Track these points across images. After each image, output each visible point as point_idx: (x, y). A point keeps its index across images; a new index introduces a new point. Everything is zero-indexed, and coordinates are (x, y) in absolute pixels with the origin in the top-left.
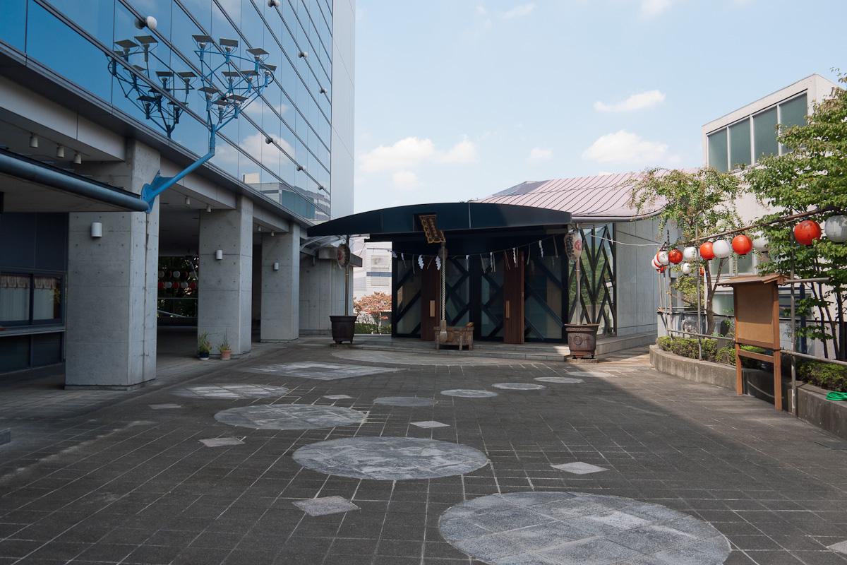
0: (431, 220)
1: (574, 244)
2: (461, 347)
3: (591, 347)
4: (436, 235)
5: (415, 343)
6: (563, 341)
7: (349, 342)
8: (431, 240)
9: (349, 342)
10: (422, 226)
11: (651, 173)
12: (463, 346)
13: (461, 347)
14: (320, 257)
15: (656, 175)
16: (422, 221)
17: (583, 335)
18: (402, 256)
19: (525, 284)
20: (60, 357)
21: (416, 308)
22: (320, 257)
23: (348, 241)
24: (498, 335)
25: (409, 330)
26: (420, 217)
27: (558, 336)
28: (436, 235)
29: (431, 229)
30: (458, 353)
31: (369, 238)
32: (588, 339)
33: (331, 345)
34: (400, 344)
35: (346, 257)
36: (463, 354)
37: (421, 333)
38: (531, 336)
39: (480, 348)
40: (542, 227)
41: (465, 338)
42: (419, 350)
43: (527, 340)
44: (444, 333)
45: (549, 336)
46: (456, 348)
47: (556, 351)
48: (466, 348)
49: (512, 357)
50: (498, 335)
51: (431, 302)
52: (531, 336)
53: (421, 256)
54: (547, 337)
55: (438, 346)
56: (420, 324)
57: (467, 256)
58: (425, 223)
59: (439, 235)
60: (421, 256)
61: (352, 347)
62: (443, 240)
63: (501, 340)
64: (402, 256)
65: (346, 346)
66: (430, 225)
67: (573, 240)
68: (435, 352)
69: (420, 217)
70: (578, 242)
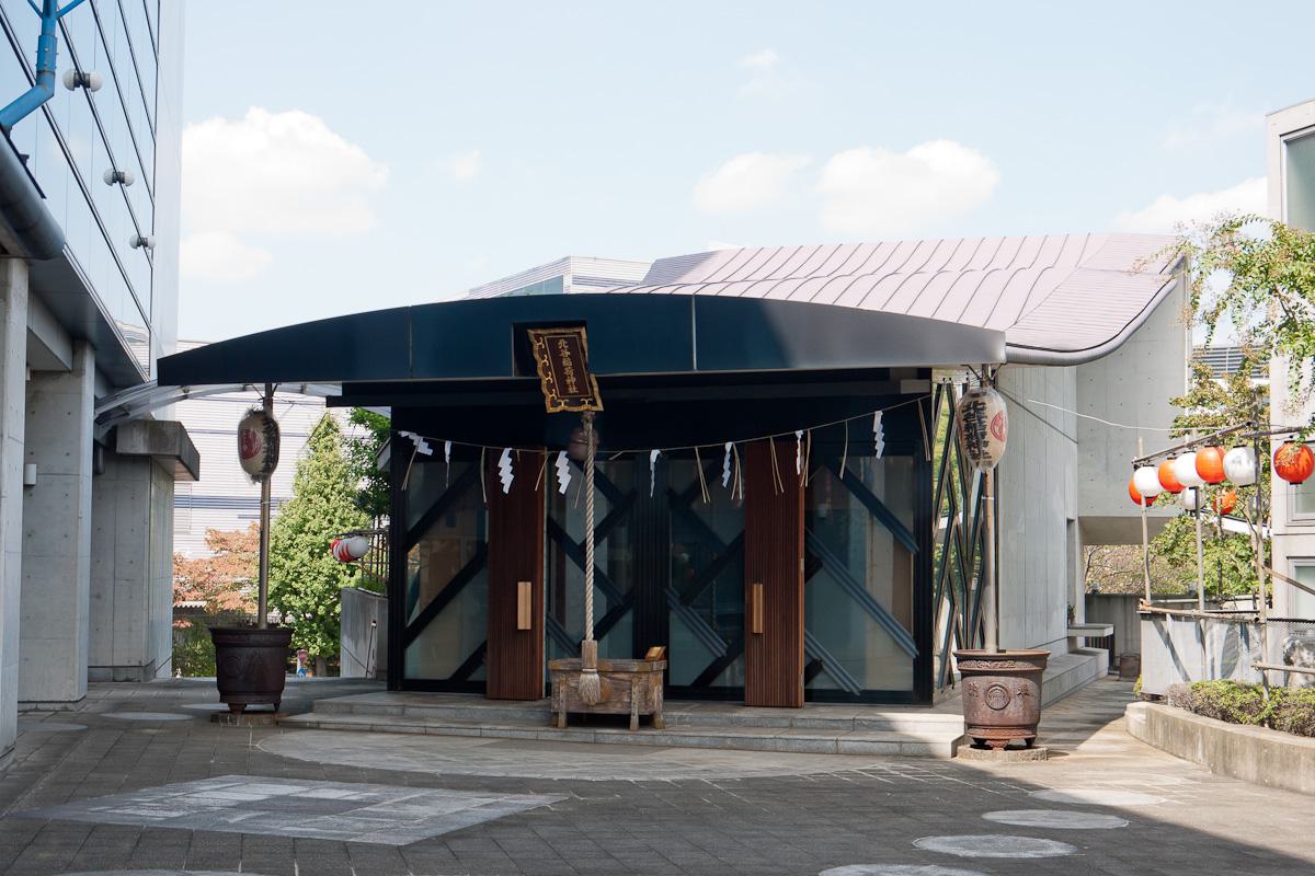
0: (562, 343)
1: (988, 422)
2: (635, 720)
3: (1032, 716)
4: (573, 390)
5: (477, 708)
6: (920, 695)
7: (271, 706)
8: (555, 404)
9: (271, 706)
10: (535, 362)
11: (1230, 228)
12: (641, 717)
13: (635, 720)
14: (119, 450)
15: (1245, 232)
16: (536, 346)
17: (1013, 684)
18: (448, 450)
19: (806, 534)
20: (549, 725)
21: (468, 607)
22: (119, 450)
23: (268, 401)
24: (475, 676)
25: (445, 669)
26: (531, 332)
27: (903, 680)
28: (573, 390)
29: (559, 370)
30: (626, 736)
31: (340, 393)
32: (1025, 693)
33: (215, 717)
34: (418, 705)
35: (268, 450)
36: (642, 739)
37: (495, 674)
38: (820, 683)
39: (681, 721)
40: (882, 374)
41: (646, 692)
42: (504, 729)
43: (812, 696)
44: (590, 679)
45: (874, 683)
46: (622, 721)
47: (887, 726)
48: (647, 721)
49: (796, 746)
50: (475, 676)
51: (521, 585)
52: (820, 683)
53: (507, 451)
54: (869, 688)
55: (562, 718)
56: (485, 643)
57: (655, 453)
58: (542, 352)
59: (583, 387)
60: (507, 451)
61: (280, 718)
62: (594, 403)
63: (736, 696)
64: (448, 450)
65: (265, 719)
66: (557, 359)
67: (987, 412)
68: (550, 734)
69: (531, 332)
70: (999, 414)
